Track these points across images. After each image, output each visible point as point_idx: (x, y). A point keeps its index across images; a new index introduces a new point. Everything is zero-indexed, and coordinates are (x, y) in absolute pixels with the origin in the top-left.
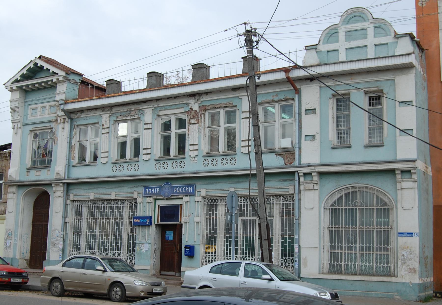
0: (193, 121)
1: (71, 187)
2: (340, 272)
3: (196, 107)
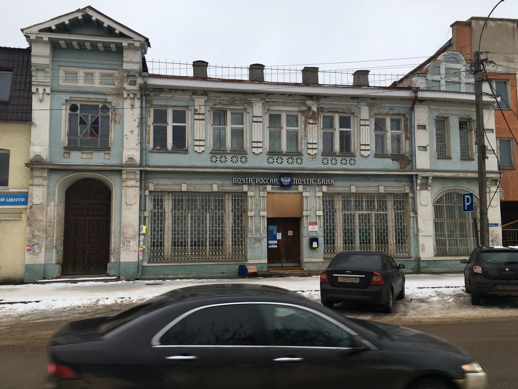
0: (311, 121)
1: (149, 176)
2: (445, 254)
3: (314, 109)
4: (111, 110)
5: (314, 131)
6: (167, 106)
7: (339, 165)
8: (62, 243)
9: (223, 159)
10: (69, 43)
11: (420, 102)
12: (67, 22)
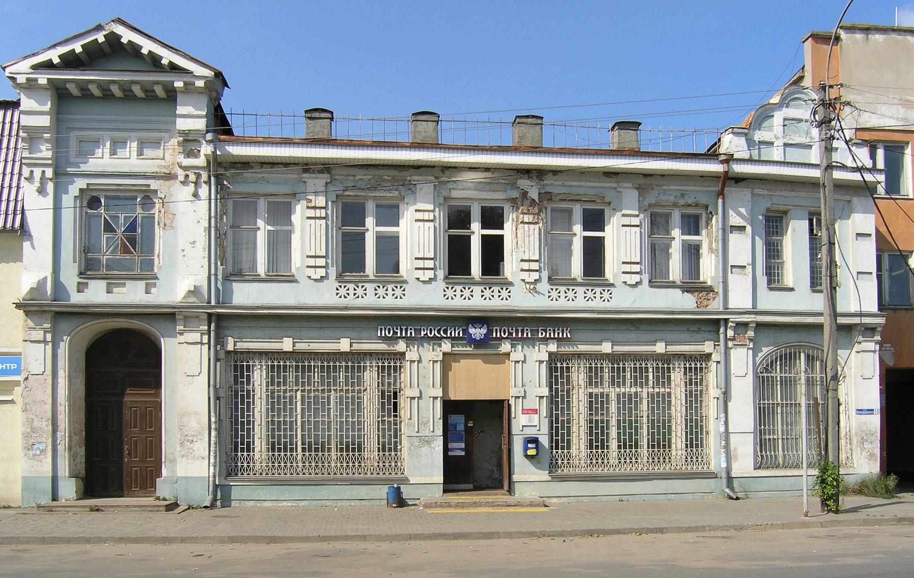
1: (224, 324)
3: (534, 194)
4: (157, 205)
5: (532, 238)
6: (257, 195)
7: (580, 301)
8: (84, 441)
9: (360, 291)
10: (83, 86)
11: (736, 182)
12: (79, 50)
